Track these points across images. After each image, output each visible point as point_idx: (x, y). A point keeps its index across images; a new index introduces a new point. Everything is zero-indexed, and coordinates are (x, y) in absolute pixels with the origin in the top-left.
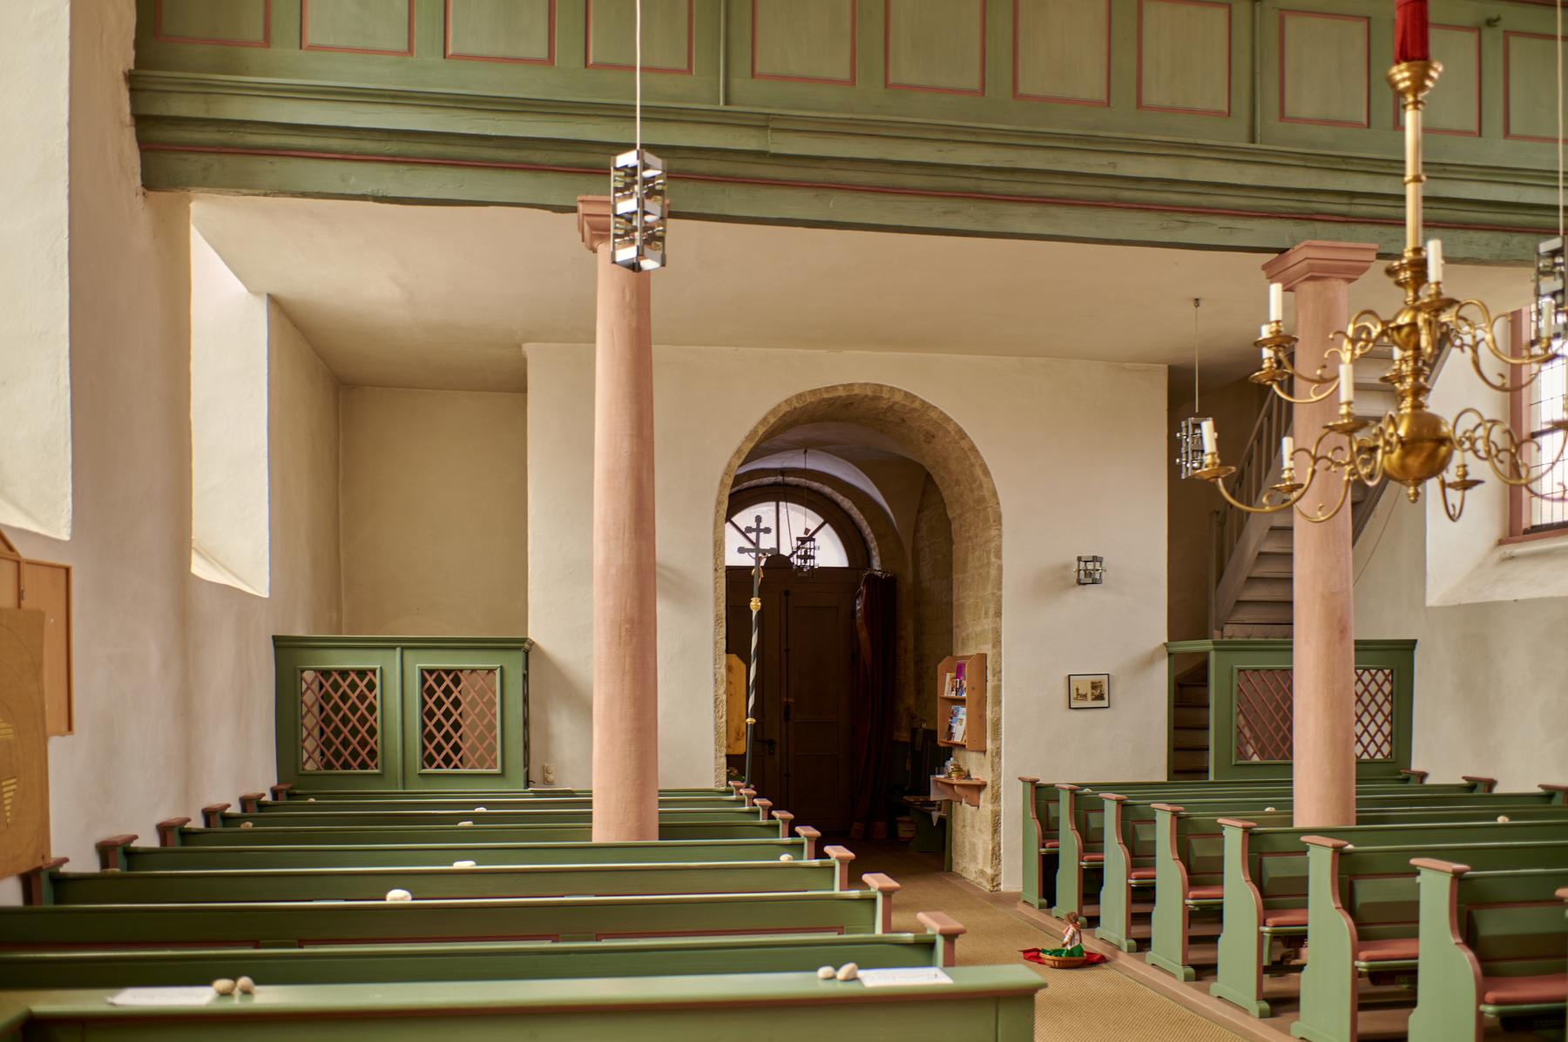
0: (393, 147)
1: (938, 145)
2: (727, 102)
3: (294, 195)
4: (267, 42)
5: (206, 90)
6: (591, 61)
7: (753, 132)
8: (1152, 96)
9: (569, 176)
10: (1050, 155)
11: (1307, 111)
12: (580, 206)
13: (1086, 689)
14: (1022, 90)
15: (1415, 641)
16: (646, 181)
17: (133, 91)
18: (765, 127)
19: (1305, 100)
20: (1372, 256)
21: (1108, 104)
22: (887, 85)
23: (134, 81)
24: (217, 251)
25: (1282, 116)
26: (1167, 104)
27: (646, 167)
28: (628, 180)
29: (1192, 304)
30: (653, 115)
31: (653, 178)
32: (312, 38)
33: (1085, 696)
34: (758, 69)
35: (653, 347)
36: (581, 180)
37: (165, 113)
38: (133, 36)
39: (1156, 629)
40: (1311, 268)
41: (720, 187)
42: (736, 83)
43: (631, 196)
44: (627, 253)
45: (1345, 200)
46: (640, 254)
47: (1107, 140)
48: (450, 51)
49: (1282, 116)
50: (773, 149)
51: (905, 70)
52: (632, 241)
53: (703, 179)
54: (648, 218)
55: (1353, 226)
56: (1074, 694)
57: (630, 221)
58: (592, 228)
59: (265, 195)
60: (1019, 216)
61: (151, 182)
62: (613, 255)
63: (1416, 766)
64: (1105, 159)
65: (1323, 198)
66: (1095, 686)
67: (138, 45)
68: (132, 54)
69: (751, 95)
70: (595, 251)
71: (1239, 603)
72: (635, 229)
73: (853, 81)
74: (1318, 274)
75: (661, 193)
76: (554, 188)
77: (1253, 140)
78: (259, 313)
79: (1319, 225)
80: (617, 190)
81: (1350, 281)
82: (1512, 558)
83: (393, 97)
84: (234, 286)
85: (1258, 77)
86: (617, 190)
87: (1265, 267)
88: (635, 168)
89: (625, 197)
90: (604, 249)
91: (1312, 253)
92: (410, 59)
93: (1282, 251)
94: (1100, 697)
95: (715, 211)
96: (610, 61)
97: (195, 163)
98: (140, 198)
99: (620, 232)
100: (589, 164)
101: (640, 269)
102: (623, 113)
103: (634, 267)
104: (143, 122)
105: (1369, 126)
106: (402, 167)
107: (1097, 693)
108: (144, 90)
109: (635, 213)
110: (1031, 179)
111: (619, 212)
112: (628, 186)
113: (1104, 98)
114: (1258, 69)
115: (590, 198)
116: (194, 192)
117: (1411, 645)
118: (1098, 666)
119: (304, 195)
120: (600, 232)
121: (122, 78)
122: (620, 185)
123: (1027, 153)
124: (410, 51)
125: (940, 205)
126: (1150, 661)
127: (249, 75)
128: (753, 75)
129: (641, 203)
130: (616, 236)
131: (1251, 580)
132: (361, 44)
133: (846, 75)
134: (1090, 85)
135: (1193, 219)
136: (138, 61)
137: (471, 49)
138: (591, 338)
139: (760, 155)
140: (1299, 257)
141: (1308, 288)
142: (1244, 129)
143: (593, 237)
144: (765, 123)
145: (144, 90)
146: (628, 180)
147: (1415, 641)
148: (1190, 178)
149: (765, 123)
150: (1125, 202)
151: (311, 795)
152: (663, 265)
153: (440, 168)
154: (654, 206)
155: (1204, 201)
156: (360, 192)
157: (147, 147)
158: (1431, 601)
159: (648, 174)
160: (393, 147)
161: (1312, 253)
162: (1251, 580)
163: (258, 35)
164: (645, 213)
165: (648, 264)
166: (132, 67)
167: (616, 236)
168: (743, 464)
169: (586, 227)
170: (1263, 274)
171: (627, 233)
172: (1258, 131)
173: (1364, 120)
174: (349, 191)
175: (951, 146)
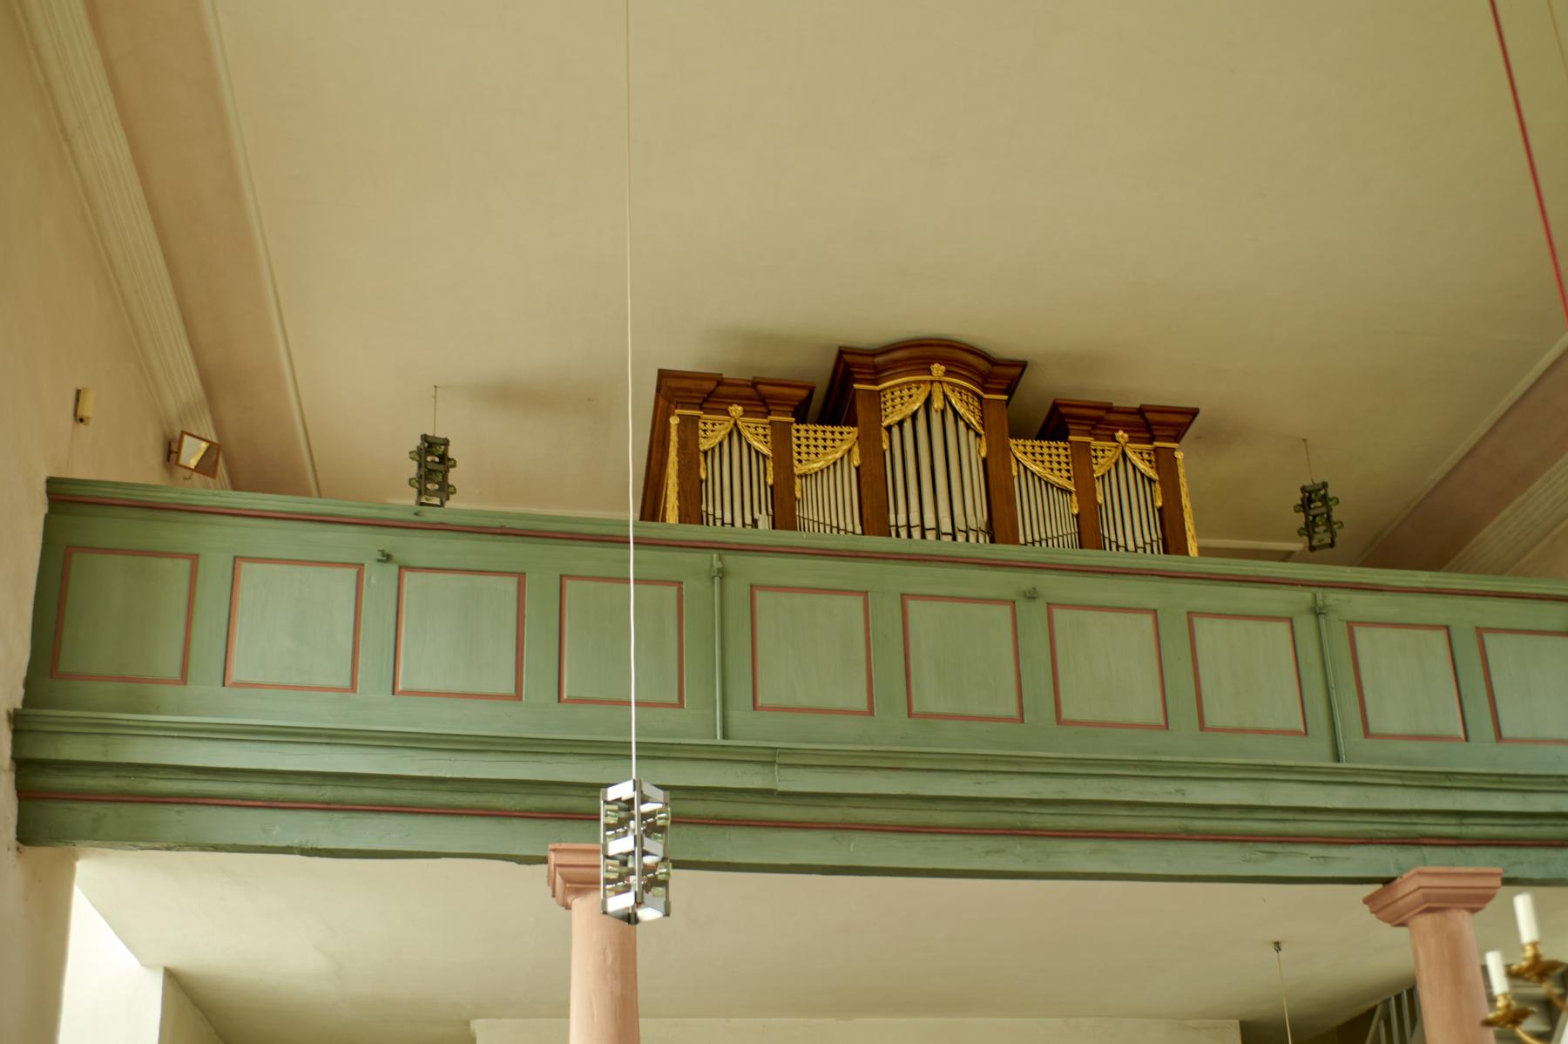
0: (328, 792)
1: (973, 776)
2: (725, 736)
3: (203, 848)
4: (184, 679)
5: (106, 730)
6: (565, 696)
7: (758, 768)
8: (1214, 718)
9: (538, 823)
10: (1106, 783)
11: (1395, 727)
12: (552, 856)
14: (1065, 715)
16: (644, 816)
17: (17, 733)
18: (772, 763)
19: (1389, 715)
20: (1497, 882)
21: (1167, 727)
22: (910, 714)
23: (19, 724)
24: (105, 917)
25: (1367, 732)
26: (1234, 724)
27: (644, 800)
28: (623, 814)
29: (1272, 948)
30: (651, 752)
31: (652, 814)
32: (236, 674)
34: (760, 701)
35: (642, 1021)
36: (553, 827)
37: (53, 756)
38: (24, 673)
40: (1426, 898)
41: (721, 830)
42: (735, 716)
43: (625, 834)
44: (621, 902)
45: (1454, 821)
46: (639, 903)
47: (1172, 765)
48: (400, 687)
49: (1367, 732)
50: (782, 787)
51: (929, 698)
52: (627, 888)
53: (717, 820)
54: (648, 860)
55: (1467, 850)
57: (624, 863)
58: (566, 880)
59: (168, 849)
60: (1077, 855)
61: (27, 835)
62: (604, 904)
64: (1171, 786)
65: (1428, 820)
67: (28, 683)
68: (21, 692)
69: (751, 729)
70: (568, 907)
72: (632, 872)
73: (870, 711)
74: (1435, 905)
75: (662, 829)
76: (522, 836)
77: (1337, 758)
78: (153, 989)
79: (1427, 851)
80: (609, 827)
81: (1473, 911)
83: (331, 736)
84: (125, 960)
85: (1333, 693)
86: (609, 827)
87: (1367, 901)
88: (630, 802)
89: (617, 837)
90: (583, 907)
91: (1425, 882)
92: (352, 695)
93: (1387, 881)
95: (713, 858)
96: (588, 695)
97: (83, 813)
98: (13, 854)
99: (613, 876)
100: (574, 809)
101: (637, 921)
102: (615, 751)
103: (630, 918)
104: (24, 766)
105: (1467, 739)
106: (336, 815)
108: (31, 731)
109: (633, 853)
110: (1087, 811)
111: (611, 853)
112: (622, 823)
113: (1161, 721)
114: (1332, 684)
115: (563, 846)
116: (80, 847)
119: (216, 848)
120: (583, 884)
121: (4, 717)
122: (612, 821)
123: (1080, 782)
124: (353, 688)
125: (981, 844)
127: (158, 711)
128: (755, 708)
129: (638, 841)
130: (608, 881)
132: (295, 681)
133: (863, 705)
134: (1146, 707)
135: (1279, 848)
136: (27, 702)
137: (423, 684)
138: (563, 1011)
139: (767, 794)
140: (1412, 885)
141: (1425, 921)
142: (1326, 749)
143: (567, 891)
144: (770, 758)
145: (31, 731)
146: (623, 814)
148: (1273, 803)
149: (770, 758)
150: (1198, 833)
151: (1488, 986)
152: (667, 914)
153: (383, 816)
154: (655, 846)
155: (1290, 828)
156: (283, 844)
157: (26, 795)
159: (646, 808)
160: (328, 792)
161: (1425, 882)
163: (175, 673)
164: (645, 853)
165: (647, 914)
166: (19, 706)
167: (608, 881)
169: (559, 879)
170: (1366, 908)
171: (621, 878)
172: (1342, 749)
173: (1461, 733)
174: (270, 843)
175: (991, 778)
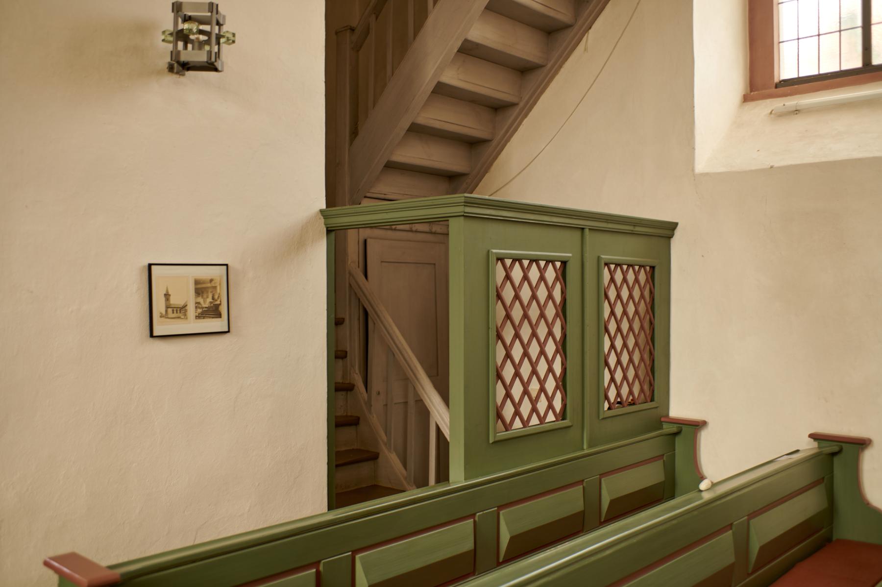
13: (184, 295)
15: (676, 224)
22: (150, 265)
33: (182, 310)
39: (305, 185)
56: (159, 306)
63: (680, 407)
66: (200, 288)
71: (391, 167)
82: (797, 111)
94: (214, 312)
107: (206, 302)
117: (670, 228)
118: (209, 247)
126: (296, 243)
131: (417, 131)
147: (676, 224)
158: (701, 166)
162: (417, 131)
168: (438, 429)
